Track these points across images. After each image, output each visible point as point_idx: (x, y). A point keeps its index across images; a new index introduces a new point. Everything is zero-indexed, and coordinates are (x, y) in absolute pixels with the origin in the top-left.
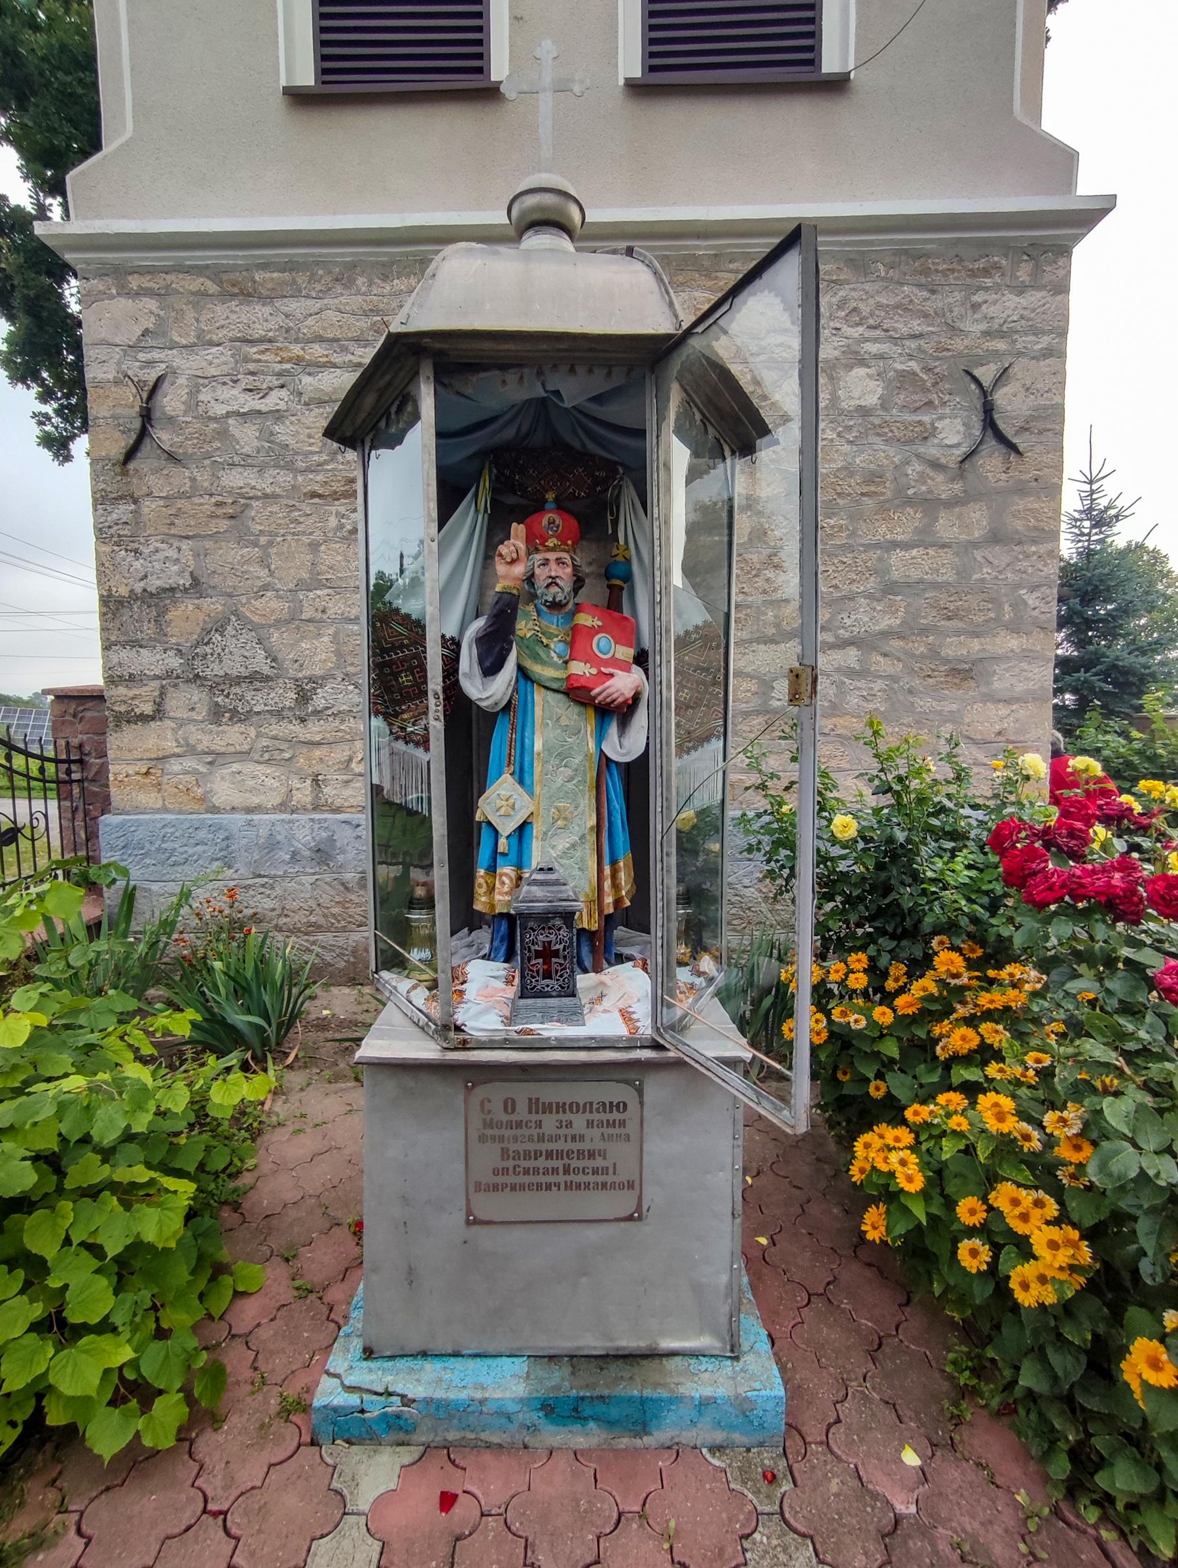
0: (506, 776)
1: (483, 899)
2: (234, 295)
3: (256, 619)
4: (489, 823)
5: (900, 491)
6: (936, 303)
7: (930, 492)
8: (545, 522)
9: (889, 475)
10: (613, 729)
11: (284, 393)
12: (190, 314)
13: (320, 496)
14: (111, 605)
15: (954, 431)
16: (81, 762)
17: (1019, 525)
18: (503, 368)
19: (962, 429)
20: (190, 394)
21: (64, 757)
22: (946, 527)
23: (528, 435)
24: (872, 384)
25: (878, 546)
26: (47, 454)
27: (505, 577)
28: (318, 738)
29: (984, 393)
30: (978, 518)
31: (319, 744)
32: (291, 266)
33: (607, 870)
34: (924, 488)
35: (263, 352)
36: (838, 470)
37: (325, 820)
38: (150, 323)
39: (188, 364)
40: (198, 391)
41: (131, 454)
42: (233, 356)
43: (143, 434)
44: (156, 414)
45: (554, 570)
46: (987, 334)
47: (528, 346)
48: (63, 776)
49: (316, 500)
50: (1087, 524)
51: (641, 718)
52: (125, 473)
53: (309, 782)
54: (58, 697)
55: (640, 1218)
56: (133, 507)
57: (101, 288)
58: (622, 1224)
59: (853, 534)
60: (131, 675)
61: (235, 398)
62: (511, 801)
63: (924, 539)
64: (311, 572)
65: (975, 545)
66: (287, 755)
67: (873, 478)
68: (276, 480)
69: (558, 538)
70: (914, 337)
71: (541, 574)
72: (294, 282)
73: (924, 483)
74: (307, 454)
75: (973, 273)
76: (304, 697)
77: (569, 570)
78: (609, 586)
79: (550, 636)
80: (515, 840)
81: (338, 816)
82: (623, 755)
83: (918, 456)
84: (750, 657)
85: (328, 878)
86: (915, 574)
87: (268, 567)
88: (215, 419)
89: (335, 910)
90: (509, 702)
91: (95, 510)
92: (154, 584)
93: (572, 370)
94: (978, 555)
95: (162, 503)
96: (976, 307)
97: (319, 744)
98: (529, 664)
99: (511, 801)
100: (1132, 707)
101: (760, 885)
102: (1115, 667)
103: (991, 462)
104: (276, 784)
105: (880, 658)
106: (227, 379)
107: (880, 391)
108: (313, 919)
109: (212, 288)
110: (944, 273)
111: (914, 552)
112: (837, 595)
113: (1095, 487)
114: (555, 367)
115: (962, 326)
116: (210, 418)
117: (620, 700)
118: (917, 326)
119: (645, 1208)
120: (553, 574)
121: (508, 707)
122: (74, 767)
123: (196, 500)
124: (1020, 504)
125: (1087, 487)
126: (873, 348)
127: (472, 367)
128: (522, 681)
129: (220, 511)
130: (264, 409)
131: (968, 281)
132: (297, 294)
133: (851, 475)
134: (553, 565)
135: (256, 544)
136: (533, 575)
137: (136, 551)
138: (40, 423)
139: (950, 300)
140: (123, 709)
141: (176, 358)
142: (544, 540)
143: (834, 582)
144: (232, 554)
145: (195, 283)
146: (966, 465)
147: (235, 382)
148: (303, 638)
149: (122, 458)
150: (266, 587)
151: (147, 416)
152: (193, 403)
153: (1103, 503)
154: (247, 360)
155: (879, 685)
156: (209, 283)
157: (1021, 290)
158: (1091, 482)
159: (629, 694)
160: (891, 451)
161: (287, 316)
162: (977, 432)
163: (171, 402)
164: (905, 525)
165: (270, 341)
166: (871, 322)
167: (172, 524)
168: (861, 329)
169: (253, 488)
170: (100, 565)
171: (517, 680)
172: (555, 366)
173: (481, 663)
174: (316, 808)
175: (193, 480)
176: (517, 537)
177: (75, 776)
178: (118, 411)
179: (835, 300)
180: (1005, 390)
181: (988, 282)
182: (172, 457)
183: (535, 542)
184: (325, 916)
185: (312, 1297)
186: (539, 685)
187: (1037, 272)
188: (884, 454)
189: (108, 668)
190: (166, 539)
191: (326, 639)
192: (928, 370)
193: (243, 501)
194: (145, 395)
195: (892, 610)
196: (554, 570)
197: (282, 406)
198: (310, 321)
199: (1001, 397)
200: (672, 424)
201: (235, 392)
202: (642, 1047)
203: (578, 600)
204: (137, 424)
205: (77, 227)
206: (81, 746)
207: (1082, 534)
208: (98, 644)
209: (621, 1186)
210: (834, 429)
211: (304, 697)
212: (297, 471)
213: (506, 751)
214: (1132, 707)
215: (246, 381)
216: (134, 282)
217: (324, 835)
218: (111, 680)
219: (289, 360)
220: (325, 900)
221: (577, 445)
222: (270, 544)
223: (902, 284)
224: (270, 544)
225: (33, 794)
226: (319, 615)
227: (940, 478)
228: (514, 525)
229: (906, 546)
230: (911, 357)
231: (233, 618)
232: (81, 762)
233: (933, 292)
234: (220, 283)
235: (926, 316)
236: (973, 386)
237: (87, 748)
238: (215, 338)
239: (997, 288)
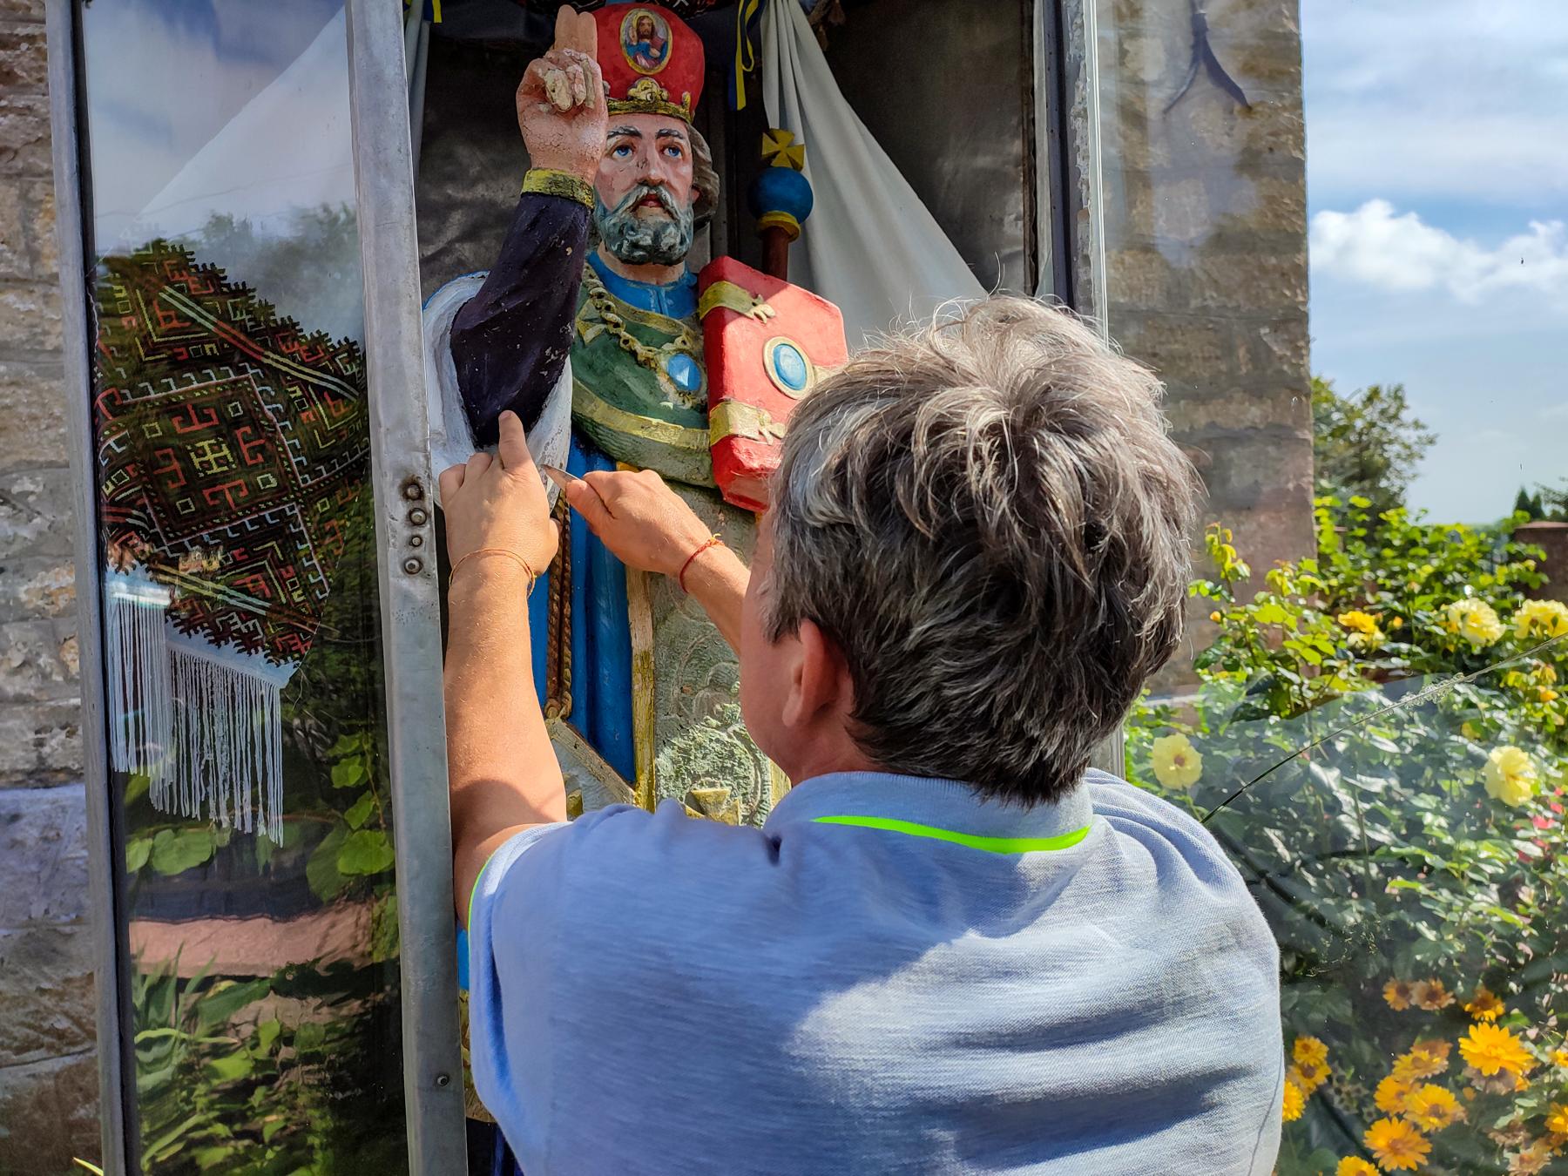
69: (661, 79)
98: (599, 411)
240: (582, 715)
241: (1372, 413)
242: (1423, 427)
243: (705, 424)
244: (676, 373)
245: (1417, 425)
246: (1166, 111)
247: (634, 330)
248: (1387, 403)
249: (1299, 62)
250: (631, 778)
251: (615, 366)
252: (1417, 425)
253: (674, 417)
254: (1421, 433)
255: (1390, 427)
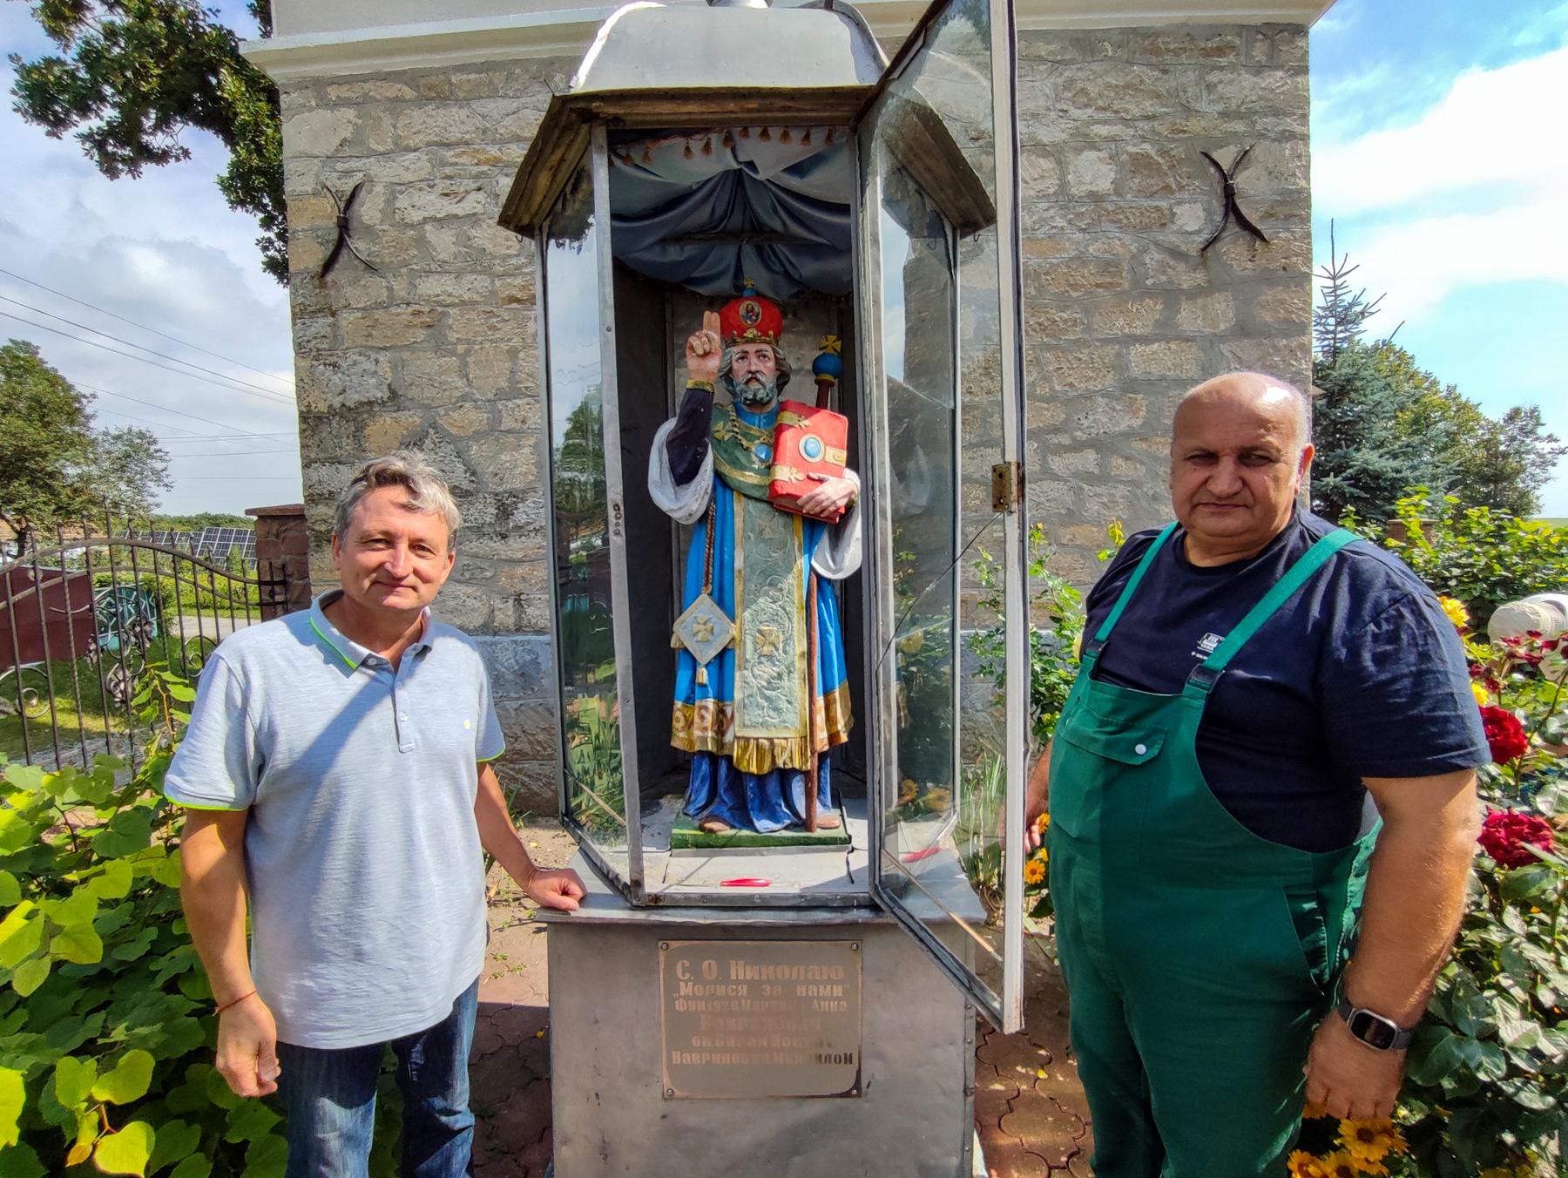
0: (704, 597)
1: (682, 735)
2: (432, 99)
3: (454, 431)
4: (686, 650)
5: (1137, 282)
6: (1171, 83)
7: (1171, 282)
8: (742, 310)
9: (1126, 266)
10: (825, 541)
11: (481, 196)
12: (387, 121)
13: (518, 301)
14: (311, 421)
15: (1193, 216)
16: (284, 583)
17: (1268, 317)
18: (687, 133)
19: (1202, 215)
20: (387, 201)
21: (268, 579)
22: (1189, 318)
23: (722, 220)
24: (1104, 168)
25: (1116, 340)
26: (272, 278)
27: (698, 371)
28: (519, 555)
29: (1225, 177)
30: (1223, 310)
31: (520, 562)
32: (487, 67)
33: (820, 701)
34: (1164, 278)
35: (459, 155)
36: (1071, 259)
37: (529, 642)
38: (347, 133)
39: (385, 172)
40: (395, 198)
41: (328, 265)
42: (429, 160)
43: (341, 244)
44: (354, 224)
45: (755, 364)
46: (1225, 115)
47: (713, 107)
48: (267, 598)
49: (515, 305)
50: (1332, 321)
51: (856, 530)
52: (323, 286)
53: (511, 602)
54: (260, 517)
55: (859, 1095)
56: (331, 319)
57: (301, 101)
58: (839, 1101)
59: (1088, 328)
60: (331, 493)
61: (431, 203)
62: (709, 625)
63: (1165, 331)
64: (509, 380)
65: (1222, 338)
66: (488, 574)
67: (1109, 266)
68: (472, 286)
69: (758, 328)
70: (1148, 118)
71: (740, 369)
72: (491, 82)
73: (1164, 273)
74: (505, 258)
75: (1207, 53)
76: (504, 512)
77: (771, 364)
78: (817, 382)
79: (751, 438)
80: (715, 669)
81: (542, 638)
82: (835, 572)
83: (1156, 244)
84: (978, 461)
85: (532, 702)
86: (1155, 370)
87: (467, 376)
88: (412, 226)
89: (541, 737)
90: (706, 513)
91: (294, 324)
92: (353, 398)
93: (765, 135)
94: (1224, 348)
95: (359, 314)
96: (1210, 87)
97: (520, 562)
98: (726, 470)
99: (709, 625)
100: (1384, 513)
101: (992, 710)
102: (1365, 471)
103: (1234, 249)
104: (478, 604)
105: (1121, 461)
106: (424, 185)
107: (1113, 175)
108: (518, 746)
109: (409, 93)
110: (1176, 53)
111: (1155, 346)
112: (1072, 394)
113: (1338, 282)
114: (745, 133)
115: (1197, 107)
116: (407, 225)
117: (832, 508)
118: (1149, 106)
119: (864, 1083)
120: (753, 368)
121: (704, 518)
122: (277, 589)
123: (393, 310)
124: (1268, 295)
125: (1330, 283)
126: (1104, 130)
127: (655, 133)
128: (720, 489)
129: (417, 321)
130: (461, 213)
131: (1202, 60)
132: (494, 94)
133: (1085, 264)
134: (754, 359)
135: (453, 353)
136: (731, 370)
137: (334, 365)
138: (265, 249)
139: (1184, 80)
140: (323, 528)
141: (374, 167)
142: (742, 330)
143: (1069, 380)
144: (428, 363)
145: (391, 90)
146: (1210, 252)
147: (431, 187)
148: (502, 450)
149: (319, 270)
150: (464, 398)
151: (344, 226)
152: (390, 211)
153: (1348, 299)
154: (444, 164)
155: (1121, 491)
156: (406, 89)
157: (1258, 70)
158: (1334, 278)
159: (842, 503)
160: (1127, 239)
161: (484, 117)
162: (1219, 218)
163: (368, 211)
164: (1144, 317)
165: (466, 143)
166: (1100, 103)
167: (370, 335)
168: (1089, 111)
169: (450, 295)
170: (300, 381)
171: (714, 489)
172: (745, 129)
173: (673, 469)
174: (519, 629)
175: (390, 289)
176: (711, 328)
177: (278, 598)
178: (318, 222)
179: (1060, 81)
180: (1246, 173)
181: (1223, 61)
182: (370, 267)
183: (730, 334)
184: (530, 743)
185: (509, 1158)
186: (740, 493)
187: (1273, 50)
188: (1122, 243)
189: (308, 486)
190: (365, 351)
191: (526, 450)
192: (1163, 153)
193: (440, 309)
194: (342, 205)
195: (1132, 409)
196: (755, 364)
197: (479, 209)
198: (508, 121)
199: (1240, 181)
200: (880, 196)
201: (432, 197)
202: (859, 907)
203: (782, 398)
204: (335, 235)
205: (277, 42)
206: (284, 567)
207: (1328, 332)
208: (298, 462)
209: (838, 1060)
210: (1063, 217)
211: (504, 512)
212: (494, 276)
213: (703, 569)
214: (1384, 513)
215: (442, 185)
216: (333, 93)
217: (528, 658)
218: (311, 499)
219: (487, 162)
220: (530, 727)
221: (778, 226)
222: (468, 352)
223: (1133, 64)
224: (468, 352)
225: (252, 613)
226: (518, 426)
227: (1181, 267)
228: (707, 313)
229: (1145, 340)
230: (1144, 139)
231: (431, 431)
232: (284, 583)
233: (1165, 72)
234: (416, 88)
235: (1158, 96)
236: (1212, 170)
237: (290, 569)
238: (412, 144)
239: (1232, 68)
240: (716, 593)
241: (1512, 430)
242: (1556, 440)
243: (769, 474)
244: (759, 452)
245: (1551, 438)
246: (1203, 250)
247: (745, 435)
248: (1524, 420)
249: (1309, 207)
250: (733, 619)
251: (733, 450)
252: (1551, 438)
253: (757, 472)
254: (1554, 445)
255: (1528, 441)
